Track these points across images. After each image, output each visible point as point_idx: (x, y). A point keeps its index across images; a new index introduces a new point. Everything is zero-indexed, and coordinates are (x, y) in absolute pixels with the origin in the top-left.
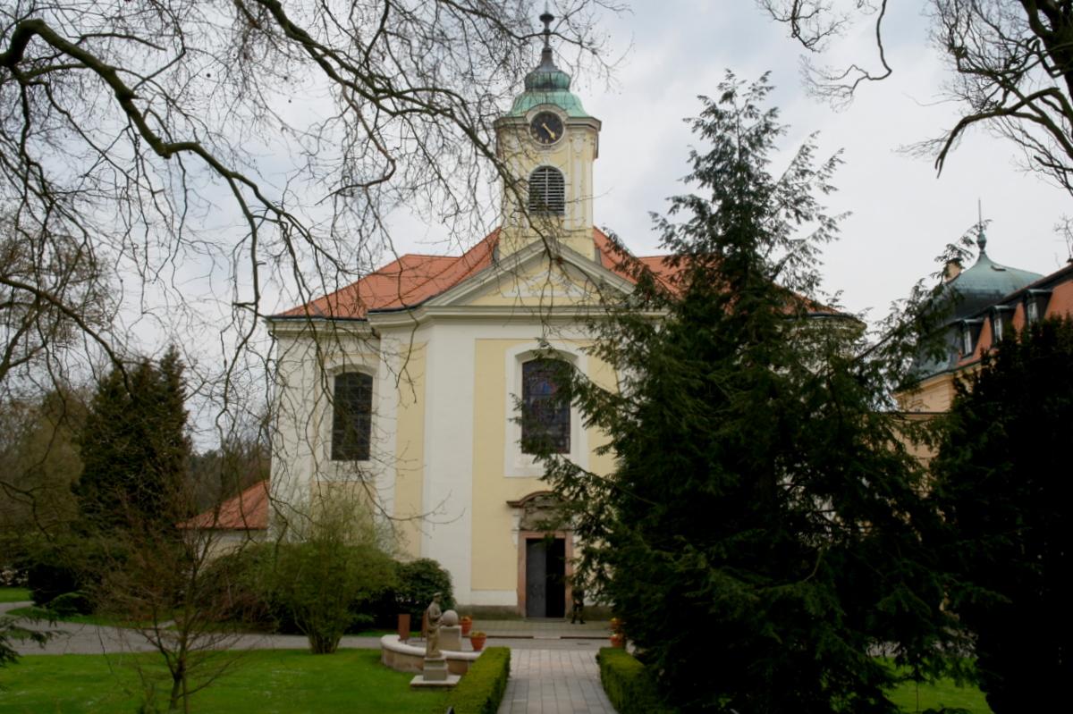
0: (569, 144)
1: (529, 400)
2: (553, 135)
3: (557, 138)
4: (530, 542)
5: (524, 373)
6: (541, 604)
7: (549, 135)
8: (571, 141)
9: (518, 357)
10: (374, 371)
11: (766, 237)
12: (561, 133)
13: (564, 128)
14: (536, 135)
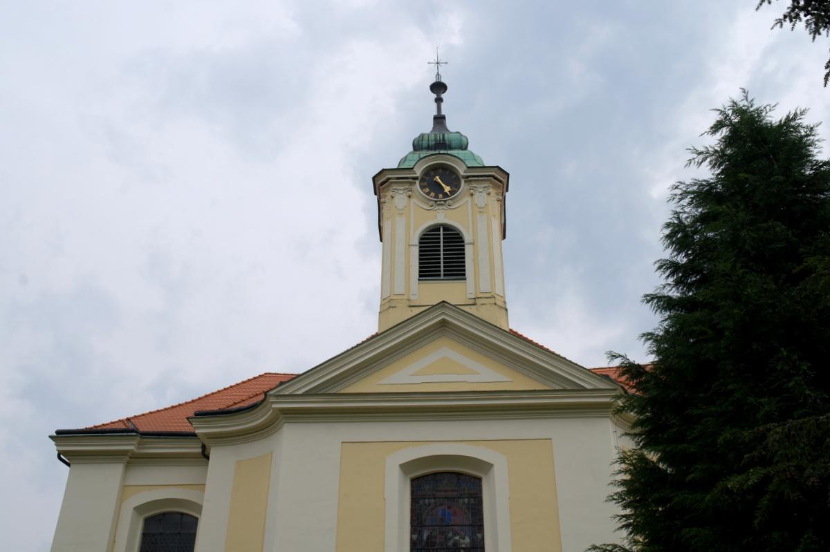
0: (468, 199)
1: (420, 534)
2: (447, 189)
3: (452, 192)
4: (415, 482)
5: (412, 492)
6: (464, 281)
7: (443, 189)
8: (472, 195)
9: (405, 467)
10: (199, 508)
11: (809, 146)
12: (458, 187)
13: (463, 181)
14: (433, 194)
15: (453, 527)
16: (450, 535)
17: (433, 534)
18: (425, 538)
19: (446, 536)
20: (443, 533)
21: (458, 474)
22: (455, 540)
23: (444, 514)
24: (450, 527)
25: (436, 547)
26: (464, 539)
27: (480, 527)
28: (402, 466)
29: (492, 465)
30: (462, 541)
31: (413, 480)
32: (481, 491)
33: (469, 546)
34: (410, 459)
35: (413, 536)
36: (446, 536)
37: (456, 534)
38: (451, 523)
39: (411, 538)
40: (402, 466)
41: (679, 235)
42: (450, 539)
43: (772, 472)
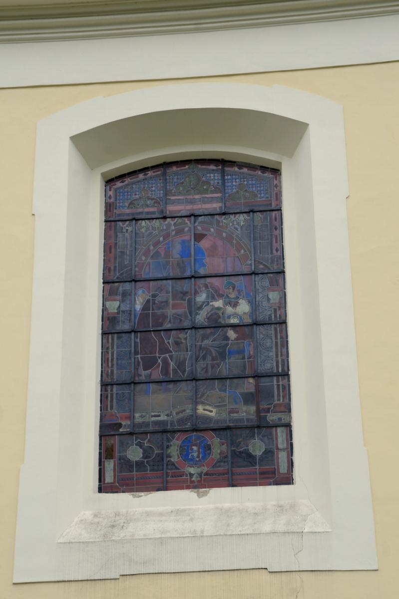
9: (89, 144)
15: (208, 280)
16: (202, 297)
17: (158, 299)
18: (138, 307)
19: (190, 301)
20: (185, 294)
21: (223, 163)
22: (213, 308)
23: (185, 252)
24: (202, 281)
25: (167, 326)
26: (235, 305)
27: (276, 274)
28: (79, 140)
29: (305, 125)
30: (229, 310)
31: (109, 181)
32: (279, 196)
33: (248, 320)
34: (102, 124)
35: (108, 304)
36: (190, 301)
37: (216, 294)
38: (202, 272)
39: (104, 309)
40: (79, 140)
41: (207, 495)
42: (200, 308)
43: (283, 420)
